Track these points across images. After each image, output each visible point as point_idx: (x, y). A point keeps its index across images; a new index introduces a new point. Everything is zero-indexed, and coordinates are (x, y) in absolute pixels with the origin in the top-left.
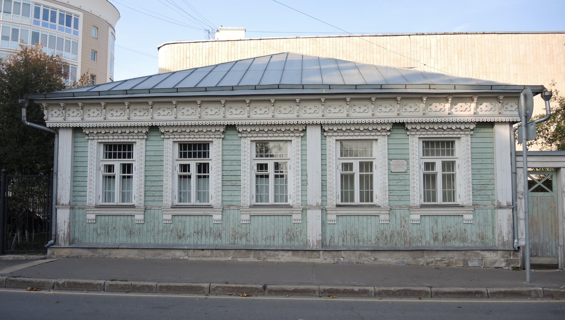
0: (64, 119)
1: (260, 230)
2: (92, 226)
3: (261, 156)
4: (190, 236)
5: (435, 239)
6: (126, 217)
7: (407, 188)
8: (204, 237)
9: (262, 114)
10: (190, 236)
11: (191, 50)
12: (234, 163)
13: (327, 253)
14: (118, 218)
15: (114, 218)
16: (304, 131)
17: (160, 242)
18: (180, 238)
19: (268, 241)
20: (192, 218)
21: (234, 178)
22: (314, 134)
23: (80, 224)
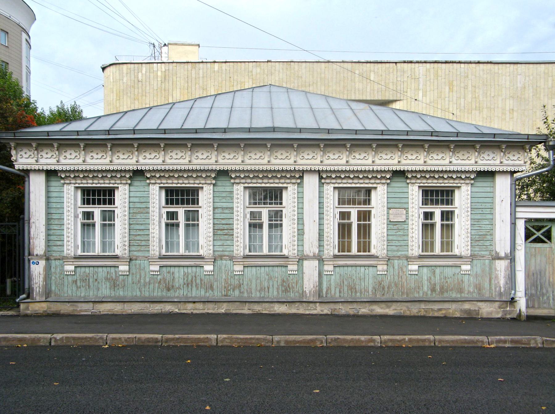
1: (254, 281)
2: (70, 278)
4: (179, 288)
5: (433, 290)
7: (405, 238)
10: (179, 288)
11: (144, 72)
15: (96, 269)
16: (301, 178)
17: (147, 294)
18: (169, 290)
21: (226, 227)
22: (311, 181)
23: (57, 276)
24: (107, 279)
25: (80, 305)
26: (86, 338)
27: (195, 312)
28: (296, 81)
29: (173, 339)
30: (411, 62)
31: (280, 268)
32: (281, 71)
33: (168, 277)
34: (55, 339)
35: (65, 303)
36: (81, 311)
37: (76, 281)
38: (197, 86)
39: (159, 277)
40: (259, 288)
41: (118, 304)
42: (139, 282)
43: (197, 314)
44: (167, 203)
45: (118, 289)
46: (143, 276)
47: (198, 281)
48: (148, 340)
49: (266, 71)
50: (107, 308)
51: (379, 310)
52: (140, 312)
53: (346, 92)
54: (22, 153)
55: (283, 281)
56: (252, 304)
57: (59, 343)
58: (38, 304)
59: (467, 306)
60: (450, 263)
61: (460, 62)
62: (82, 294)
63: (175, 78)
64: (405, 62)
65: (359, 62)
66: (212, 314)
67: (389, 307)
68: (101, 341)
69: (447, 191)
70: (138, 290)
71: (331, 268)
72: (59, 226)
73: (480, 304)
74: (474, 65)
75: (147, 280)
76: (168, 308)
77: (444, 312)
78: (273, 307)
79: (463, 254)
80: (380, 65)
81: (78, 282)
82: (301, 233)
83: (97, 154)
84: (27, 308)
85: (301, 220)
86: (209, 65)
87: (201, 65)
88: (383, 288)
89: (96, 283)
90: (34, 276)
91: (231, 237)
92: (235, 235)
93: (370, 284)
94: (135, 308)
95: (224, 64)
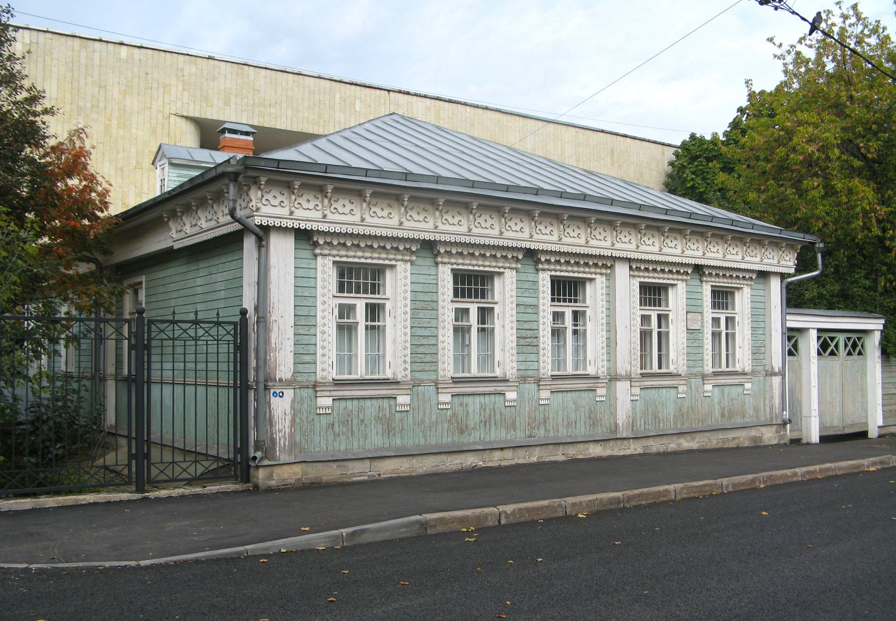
0: (292, 213)
1: (561, 413)
2: (324, 420)
3: (559, 300)
4: (474, 429)
5: (723, 415)
6: (380, 401)
7: (700, 350)
8: (493, 428)
9: (575, 239)
10: (474, 429)
12: (530, 310)
13: (636, 441)
14: (368, 403)
15: (362, 402)
16: (612, 267)
17: (433, 441)
18: (462, 432)
19: (570, 430)
20: (477, 397)
21: (529, 333)
22: (282, 249)
23: (304, 417)
24: (378, 419)
25: (350, 465)
26: (542, 508)
27: (504, 463)
28: (250, 96)
29: (634, 496)
30: (408, 93)
31: (586, 393)
32: (229, 76)
33: (460, 411)
34: (505, 512)
35: (329, 464)
36: (353, 475)
37: (333, 425)
38: (89, 79)
39: (449, 412)
40: (566, 423)
41: (405, 460)
42: (423, 421)
43: (506, 467)
44: (456, 295)
45: (394, 434)
46: (428, 412)
47: (498, 417)
48: (611, 501)
49: (205, 72)
50: (389, 468)
51: (686, 444)
52: (434, 470)
53: (321, 123)
54: (269, 197)
55: (591, 412)
56: (566, 446)
57: (512, 520)
58: (285, 468)
59: (754, 433)
60: (492, 389)
61: (465, 104)
62: (342, 446)
63: (48, 58)
64: (400, 92)
65: (340, 82)
66: (524, 465)
67: (693, 439)
68: (559, 509)
69: (723, 292)
70: (421, 435)
71: (328, 402)
72: (307, 328)
73: (763, 429)
74: (480, 111)
75: (434, 418)
76: (470, 460)
77: (736, 441)
78: (588, 449)
79: (399, 378)
80: (368, 90)
81: (336, 426)
82: (611, 344)
83: (383, 209)
84: (270, 477)
85: (611, 326)
86: (111, 46)
87: (97, 44)
88: (683, 416)
89: (362, 427)
90: (276, 417)
91: (535, 348)
92: (541, 346)
93: (669, 411)
94: (427, 465)
95: (136, 50)
